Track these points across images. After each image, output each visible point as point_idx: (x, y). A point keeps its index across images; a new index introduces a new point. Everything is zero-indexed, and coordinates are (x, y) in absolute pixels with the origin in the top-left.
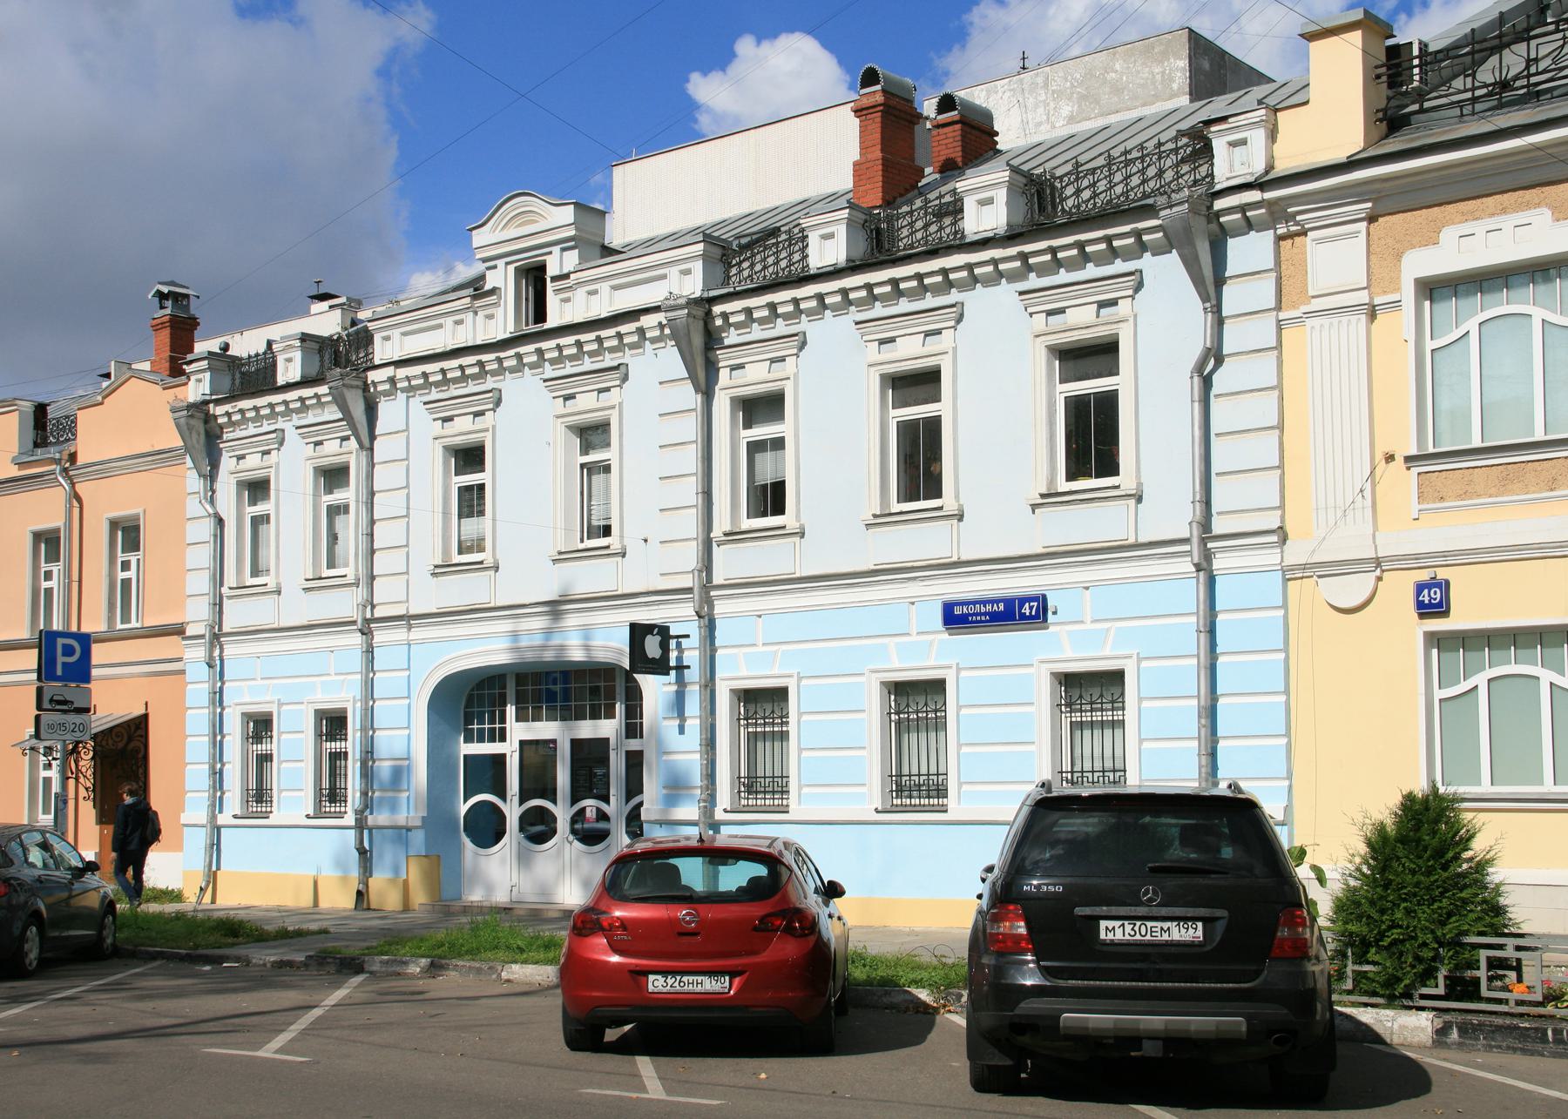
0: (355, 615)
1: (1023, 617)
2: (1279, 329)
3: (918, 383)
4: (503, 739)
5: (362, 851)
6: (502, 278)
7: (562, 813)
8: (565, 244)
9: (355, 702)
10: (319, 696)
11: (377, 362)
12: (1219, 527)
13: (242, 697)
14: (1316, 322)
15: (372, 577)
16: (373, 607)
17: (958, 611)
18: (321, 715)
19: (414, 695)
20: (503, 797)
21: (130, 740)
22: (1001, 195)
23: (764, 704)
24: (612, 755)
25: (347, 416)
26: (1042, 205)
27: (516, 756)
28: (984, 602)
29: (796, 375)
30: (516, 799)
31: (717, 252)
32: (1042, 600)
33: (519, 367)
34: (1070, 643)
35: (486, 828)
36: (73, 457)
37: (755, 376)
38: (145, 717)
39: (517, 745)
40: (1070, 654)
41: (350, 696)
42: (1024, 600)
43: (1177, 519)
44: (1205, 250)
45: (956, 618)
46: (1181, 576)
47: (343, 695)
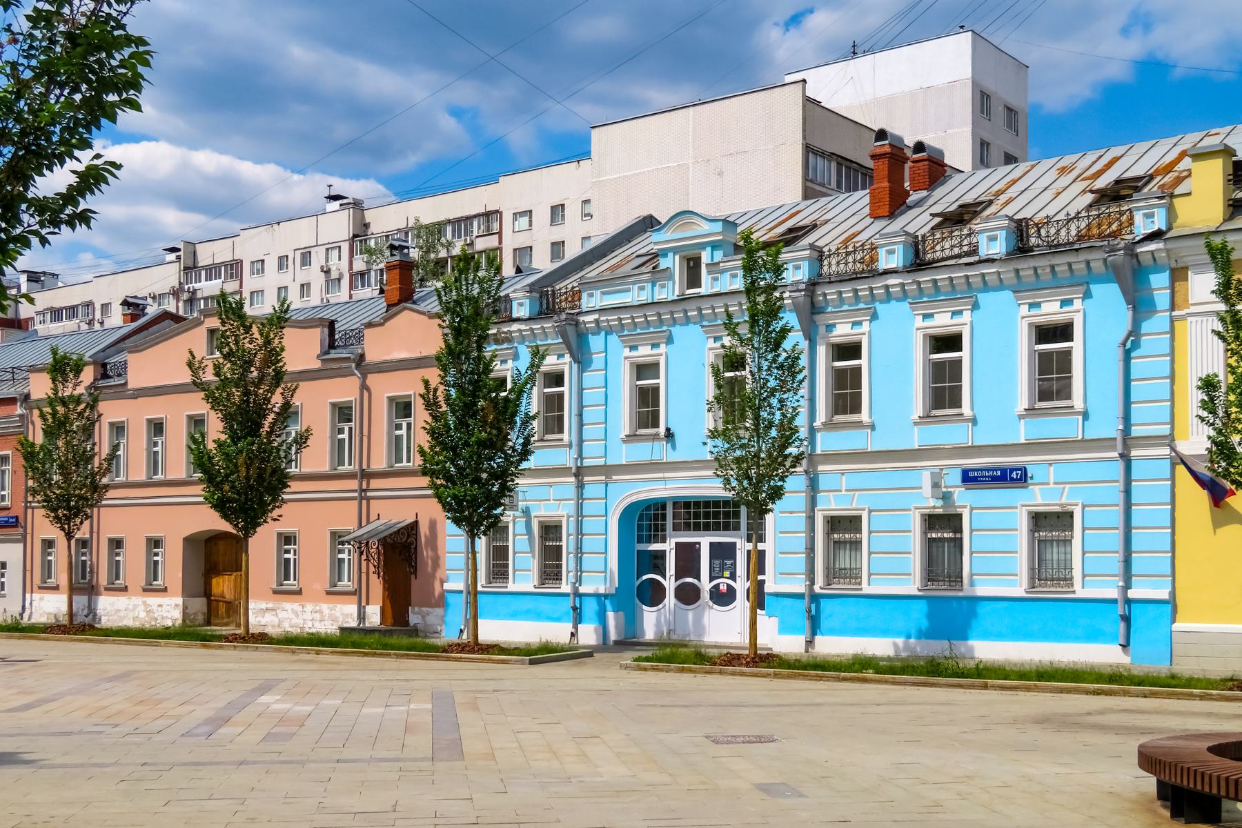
0: (571, 464)
1: (1012, 479)
2: (1172, 322)
3: (950, 342)
4: (664, 541)
5: (575, 608)
6: (673, 263)
7: (705, 584)
8: (715, 246)
9: (569, 517)
10: (543, 513)
11: (585, 309)
12: (1136, 431)
13: (830, 504)
14: (1193, 319)
15: (581, 441)
16: (582, 459)
17: (971, 474)
18: (149, 540)
19: (610, 514)
20: (664, 577)
21: (409, 536)
22: (1002, 235)
23: (844, 527)
24: (738, 552)
25: (566, 342)
26: (1022, 240)
27: (673, 552)
28: (988, 470)
29: (870, 332)
30: (673, 578)
31: (816, 254)
32: (1024, 471)
33: (687, 320)
34: (1040, 497)
35: (653, 595)
36: (362, 356)
37: (843, 331)
38: (416, 522)
39: (673, 545)
40: (1040, 501)
41: (565, 513)
42: (1012, 470)
43: (1108, 427)
44: (1132, 280)
45: (970, 478)
46: (1111, 459)
47: (560, 513)
